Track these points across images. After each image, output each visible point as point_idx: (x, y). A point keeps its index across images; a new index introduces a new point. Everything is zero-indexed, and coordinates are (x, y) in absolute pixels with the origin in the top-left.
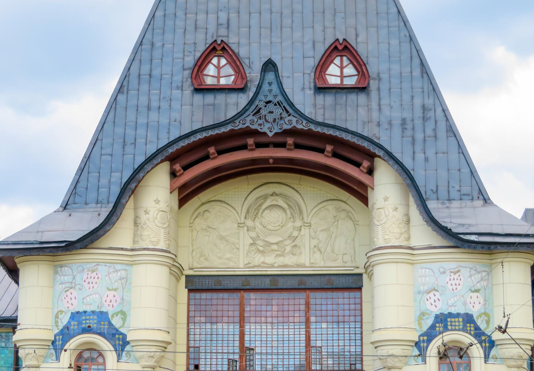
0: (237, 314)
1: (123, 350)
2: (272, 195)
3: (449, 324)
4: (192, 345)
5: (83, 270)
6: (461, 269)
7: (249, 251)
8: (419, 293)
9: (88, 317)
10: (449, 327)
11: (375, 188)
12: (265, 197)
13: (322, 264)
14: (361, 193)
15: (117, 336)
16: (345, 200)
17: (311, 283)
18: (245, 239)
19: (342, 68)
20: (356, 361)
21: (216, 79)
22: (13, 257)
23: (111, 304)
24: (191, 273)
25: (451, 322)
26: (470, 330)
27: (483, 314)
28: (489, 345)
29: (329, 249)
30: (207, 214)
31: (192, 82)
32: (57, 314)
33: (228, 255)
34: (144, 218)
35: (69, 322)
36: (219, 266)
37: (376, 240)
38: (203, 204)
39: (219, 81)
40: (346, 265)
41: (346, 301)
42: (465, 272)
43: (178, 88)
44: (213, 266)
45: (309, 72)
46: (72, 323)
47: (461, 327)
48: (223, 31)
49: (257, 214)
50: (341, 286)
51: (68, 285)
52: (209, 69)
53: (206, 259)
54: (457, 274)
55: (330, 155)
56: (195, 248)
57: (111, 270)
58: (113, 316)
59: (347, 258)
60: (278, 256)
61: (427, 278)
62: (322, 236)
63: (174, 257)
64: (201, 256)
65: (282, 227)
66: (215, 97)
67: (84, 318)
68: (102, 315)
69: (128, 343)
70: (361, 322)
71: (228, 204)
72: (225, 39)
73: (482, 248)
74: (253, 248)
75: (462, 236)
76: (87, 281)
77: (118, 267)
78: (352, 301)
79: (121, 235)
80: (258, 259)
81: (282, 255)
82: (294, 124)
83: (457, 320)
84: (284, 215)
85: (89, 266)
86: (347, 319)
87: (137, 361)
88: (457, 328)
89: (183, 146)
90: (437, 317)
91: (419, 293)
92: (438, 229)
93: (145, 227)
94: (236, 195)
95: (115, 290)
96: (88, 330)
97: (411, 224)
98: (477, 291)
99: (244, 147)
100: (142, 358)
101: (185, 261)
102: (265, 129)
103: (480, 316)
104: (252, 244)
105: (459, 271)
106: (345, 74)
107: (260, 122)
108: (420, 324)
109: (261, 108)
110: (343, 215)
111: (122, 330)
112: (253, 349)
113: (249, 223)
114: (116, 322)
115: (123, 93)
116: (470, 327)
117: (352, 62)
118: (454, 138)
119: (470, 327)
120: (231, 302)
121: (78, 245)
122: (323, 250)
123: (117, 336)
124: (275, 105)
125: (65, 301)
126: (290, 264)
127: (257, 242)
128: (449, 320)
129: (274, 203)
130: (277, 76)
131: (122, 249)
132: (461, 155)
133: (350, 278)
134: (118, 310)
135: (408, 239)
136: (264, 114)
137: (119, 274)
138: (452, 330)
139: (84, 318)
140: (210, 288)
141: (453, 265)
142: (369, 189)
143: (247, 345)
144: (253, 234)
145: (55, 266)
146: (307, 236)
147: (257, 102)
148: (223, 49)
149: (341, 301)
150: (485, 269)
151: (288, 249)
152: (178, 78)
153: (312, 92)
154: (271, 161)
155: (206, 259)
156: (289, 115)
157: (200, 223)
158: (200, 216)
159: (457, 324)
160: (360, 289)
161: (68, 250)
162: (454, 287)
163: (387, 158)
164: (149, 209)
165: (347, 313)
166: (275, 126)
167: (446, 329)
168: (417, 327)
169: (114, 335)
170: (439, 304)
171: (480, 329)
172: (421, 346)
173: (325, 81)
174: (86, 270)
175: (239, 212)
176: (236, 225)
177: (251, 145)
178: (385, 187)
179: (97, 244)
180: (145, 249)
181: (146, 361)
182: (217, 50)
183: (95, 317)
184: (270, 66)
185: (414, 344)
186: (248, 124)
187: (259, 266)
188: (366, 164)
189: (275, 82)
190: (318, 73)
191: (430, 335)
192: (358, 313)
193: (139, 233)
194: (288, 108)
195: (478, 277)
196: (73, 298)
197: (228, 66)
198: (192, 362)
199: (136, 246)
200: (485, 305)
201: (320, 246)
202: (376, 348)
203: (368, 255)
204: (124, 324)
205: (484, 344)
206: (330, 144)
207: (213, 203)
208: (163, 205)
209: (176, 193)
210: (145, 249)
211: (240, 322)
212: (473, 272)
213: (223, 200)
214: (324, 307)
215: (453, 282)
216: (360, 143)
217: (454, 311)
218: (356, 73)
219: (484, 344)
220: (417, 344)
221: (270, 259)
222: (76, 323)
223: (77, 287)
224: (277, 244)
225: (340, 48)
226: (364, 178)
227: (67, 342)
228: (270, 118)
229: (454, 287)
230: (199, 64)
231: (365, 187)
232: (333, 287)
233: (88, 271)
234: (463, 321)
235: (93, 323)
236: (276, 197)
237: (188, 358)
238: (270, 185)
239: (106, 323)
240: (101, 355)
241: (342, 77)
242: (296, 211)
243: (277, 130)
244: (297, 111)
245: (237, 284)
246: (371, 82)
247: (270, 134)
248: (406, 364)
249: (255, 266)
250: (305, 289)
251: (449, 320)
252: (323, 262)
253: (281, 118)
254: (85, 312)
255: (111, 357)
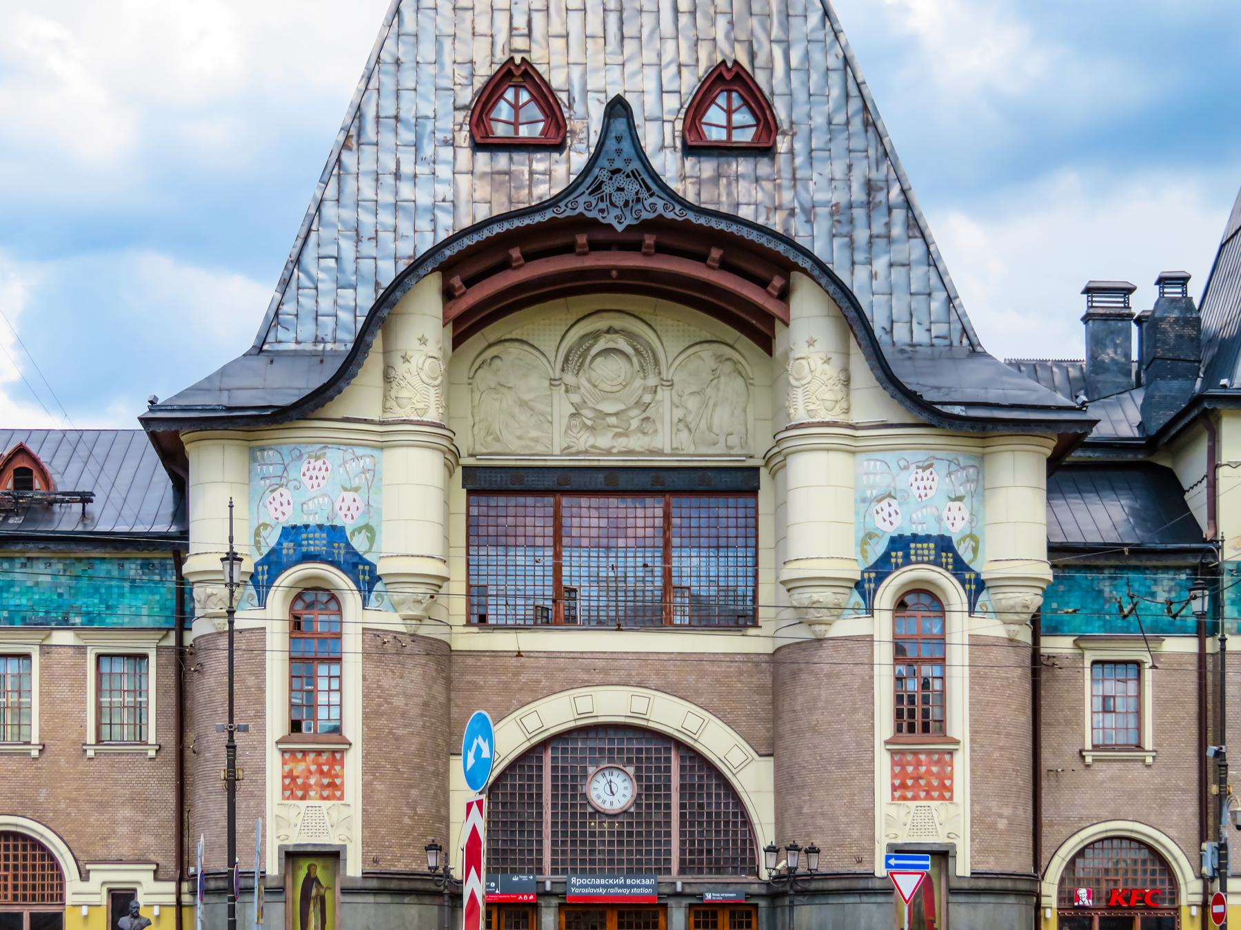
0: (550, 531)
1: (370, 591)
2: (608, 332)
3: (912, 552)
4: (475, 583)
5: (301, 455)
6: (935, 462)
7: (569, 427)
8: (864, 500)
9: (311, 535)
10: (913, 558)
11: (791, 323)
12: (595, 335)
13: (692, 450)
14: (761, 331)
15: (361, 567)
16: (730, 342)
17: (672, 481)
18: (562, 406)
19: (729, 112)
20: (516, 590)
21: (512, 127)
22: (177, 433)
23: (349, 514)
24: (471, 462)
25: (916, 549)
26: (947, 563)
27: (967, 536)
28: (977, 587)
29: (703, 425)
30: (497, 361)
31: (470, 131)
32: (258, 528)
33: (534, 434)
34: (401, 369)
35: (279, 543)
36: (518, 452)
37: (792, 411)
38: (490, 345)
39: (516, 131)
40: (732, 452)
41: (732, 512)
42: (941, 468)
43: (446, 143)
44: (508, 451)
45: (672, 117)
46: (285, 545)
47: (932, 558)
48: (520, 43)
49: (582, 363)
50: (723, 487)
51: (277, 481)
52: (500, 110)
53: (497, 440)
54: (928, 471)
55: (717, 265)
56: (477, 420)
57: (349, 456)
58: (353, 534)
59: (733, 440)
60: (617, 435)
61: (878, 477)
62: (693, 403)
63: (451, 435)
64: (488, 433)
65: (625, 386)
66: (511, 159)
67: (304, 536)
68: (335, 532)
69: (379, 578)
70: (756, 547)
71: (533, 346)
72: (526, 56)
73: (973, 428)
74: (576, 422)
75: (939, 407)
76: (308, 475)
77: (359, 451)
78: (741, 512)
79: (363, 397)
80: (584, 440)
81: (625, 434)
82: (660, 210)
83: (925, 545)
84: (628, 366)
85: (310, 448)
86: (732, 542)
87: (395, 607)
88: (926, 559)
89: (469, 246)
90: (893, 540)
91: (864, 500)
92: (900, 396)
93: (403, 384)
94: (548, 331)
95: (356, 490)
96: (308, 558)
97: (853, 385)
98: (959, 499)
99: (569, 249)
100: (403, 602)
101: (464, 443)
102: (610, 219)
103: (963, 539)
104: (573, 415)
105: (931, 466)
106: (735, 124)
107: (602, 205)
108: (864, 552)
109: (602, 182)
110: (728, 367)
111: (368, 557)
112: (575, 590)
113: (569, 378)
114: (359, 543)
115: (350, 149)
116: (947, 557)
117: (746, 103)
118: (920, 241)
119: (947, 557)
120: (539, 512)
121: (292, 413)
122: (692, 426)
123: (361, 567)
124: (628, 176)
125: (271, 508)
126: (638, 449)
127: (583, 412)
128: (912, 545)
129: (611, 345)
130: (632, 127)
131: (365, 421)
132: (932, 269)
133: (739, 474)
134: (362, 523)
135: (847, 411)
136: (607, 191)
137: (362, 462)
138: (917, 562)
139: (304, 536)
140: (504, 487)
141: (921, 456)
142: (778, 324)
143: (566, 583)
144: (576, 398)
145: (252, 449)
146: (667, 403)
147: (596, 171)
148: (525, 74)
149: (722, 512)
150: (972, 463)
151: (635, 424)
152: (446, 123)
153: (679, 154)
154: (614, 273)
155: (497, 440)
156: (651, 195)
157: (486, 378)
158: (485, 366)
159: (926, 552)
160: (754, 492)
161: (273, 422)
162: (923, 492)
163: (816, 273)
164: (409, 353)
165: (732, 532)
166: (628, 214)
167: (907, 561)
168: (859, 557)
169: (355, 565)
170: (897, 520)
171: (962, 561)
172: (865, 588)
173: (700, 135)
174: (306, 456)
175: (552, 360)
176: (547, 383)
177: (582, 246)
178: (808, 325)
179: (322, 412)
180: (405, 422)
181: (409, 608)
182: (513, 75)
183: (324, 535)
184: (618, 108)
185: (852, 585)
186: (580, 209)
187: (586, 452)
188: (777, 282)
189: (626, 135)
190: (689, 121)
191: (882, 569)
192: (751, 531)
193: (393, 394)
194: (649, 182)
195: (962, 475)
196: (285, 503)
197: (532, 103)
198: (475, 610)
199: (389, 416)
200: (971, 522)
201: (689, 419)
202: (789, 590)
203: (778, 437)
204: (371, 547)
205: (967, 587)
206: (718, 246)
207: (507, 344)
208: (432, 348)
209: (450, 326)
210: (405, 422)
211: (555, 546)
212: (953, 467)
213: (525, 338)
214: (694, 523)
215: (921, 484)
216: (771, 246)
217: (921, 531)
218: (753, 122)
219: (967, 587)
220: (858, 585)
221: (604, 441)
222: (292, 544)
223: (291, 484)
224: (616, 414)
225: (728, 76)
226: (771, 306)
227: (277, 576)
228: (619, 199)
229: (923, 492)
230: (483, 99)
231: (769, 319)
232: (711, 488)
233: (309, 457)
234: (935, 548)
235: (317, 544)
236: (615, 336)
237: (469, 605)
238: (605, 314)
239: (342, 545)
240: (333, 597)
241: (730, 128)
242: (647, 358)
243: (629, 220)
244: (664, 187)
245: (550, 482)
246: (779, 138)
247: (620, 228)
248: (838, 617)
249: (578, 453)
250: (662, 493)
251: (912, 545)
252: (692, 447)
253: (638, 200)
254: (306, 526)
255: (351, 601)
